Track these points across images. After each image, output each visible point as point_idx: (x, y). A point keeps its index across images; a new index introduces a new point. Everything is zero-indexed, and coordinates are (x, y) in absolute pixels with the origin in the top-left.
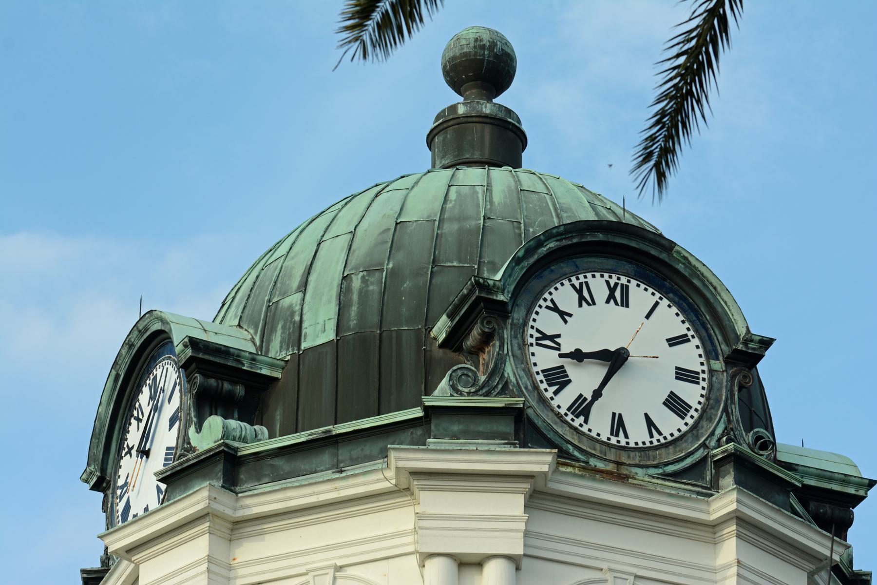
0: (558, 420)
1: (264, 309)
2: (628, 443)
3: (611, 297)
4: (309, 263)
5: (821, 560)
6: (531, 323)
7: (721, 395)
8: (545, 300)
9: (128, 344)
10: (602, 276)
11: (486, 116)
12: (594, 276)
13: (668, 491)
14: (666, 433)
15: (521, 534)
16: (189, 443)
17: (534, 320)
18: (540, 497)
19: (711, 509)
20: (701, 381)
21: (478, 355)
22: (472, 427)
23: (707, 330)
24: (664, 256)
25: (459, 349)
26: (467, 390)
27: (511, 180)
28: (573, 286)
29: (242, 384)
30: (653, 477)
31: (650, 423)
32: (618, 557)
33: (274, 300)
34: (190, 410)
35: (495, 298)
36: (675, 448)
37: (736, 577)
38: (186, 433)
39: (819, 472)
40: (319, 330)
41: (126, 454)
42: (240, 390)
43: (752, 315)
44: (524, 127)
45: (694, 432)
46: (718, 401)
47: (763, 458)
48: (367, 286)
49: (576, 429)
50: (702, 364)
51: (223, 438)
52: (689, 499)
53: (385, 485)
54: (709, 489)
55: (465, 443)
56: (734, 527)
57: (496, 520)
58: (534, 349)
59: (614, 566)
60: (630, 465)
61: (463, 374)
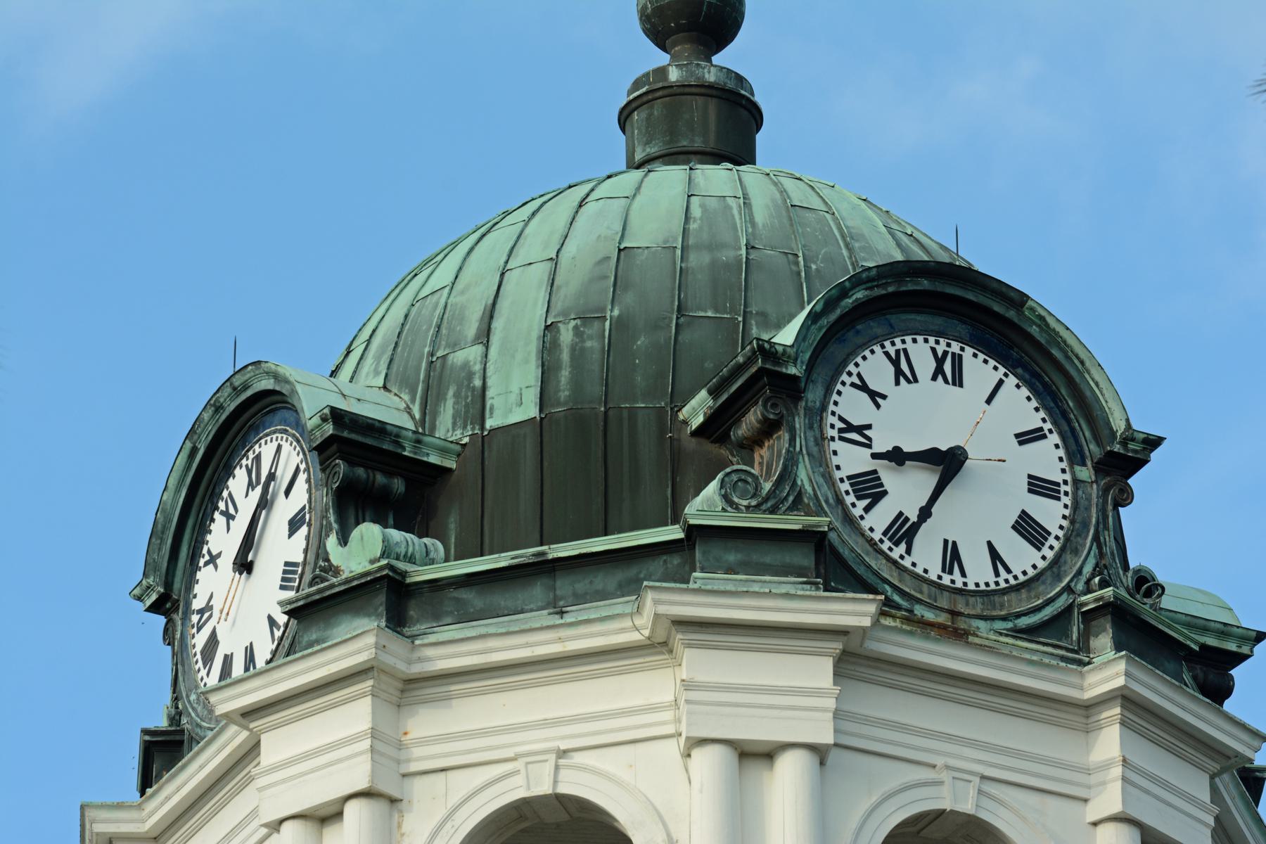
0: (870, 549)
1: (424, 365)
2: (965, 584)
3: (939, 371)
4: (490, 301)
5: (1229, 758)
6: (832, 407)
7: (1090, 517)
8: (850, 374)
9: (214, 405)
10: (926, 341)
11: (711, 86)
12: (915, 341)
13: (1028, 656)
14: (1017, 570)
15: (831, 715)
16: (327, 560)
17: (836, 403)
18: (854, 660)
19: (1086, 684)
20: (1062, 495)
21: (752, 450)
22: (755, 557)
23: (1069, 421)
24: (1011, 314)
25: (723, 439)
26: (745, 503)
27: (773, 188)
28: (887, 354)
29: (401, 476)
30: (1001, 634)
31: (995, 556)
32: (968, 752)
33: (439, 354)
34: (327, 511)
35: (784, 370)
36: (1029, 591)
37: (1119, 783)
38: (321, 545)
39: (1189, 619)
40: (514, 400)
41: (206, 564)
42: (398, 485)
43: (1132, 403)
44: (758, 98)
45: (1055, 570)
46: (1086, 525)
47: (1147, 607)
48: (583, 341)
49: (895, 562)
50: (1063, 471)
51: (383, 555)
52: (1057, 668)
53: (634, 637)
54: (1076, 652)
55: (747, 581)
56: (1118, 710)
57: (795, 693)
58: (837, 445)
59: (952, 762)
60: (969, 616)
61: (740, 480)
